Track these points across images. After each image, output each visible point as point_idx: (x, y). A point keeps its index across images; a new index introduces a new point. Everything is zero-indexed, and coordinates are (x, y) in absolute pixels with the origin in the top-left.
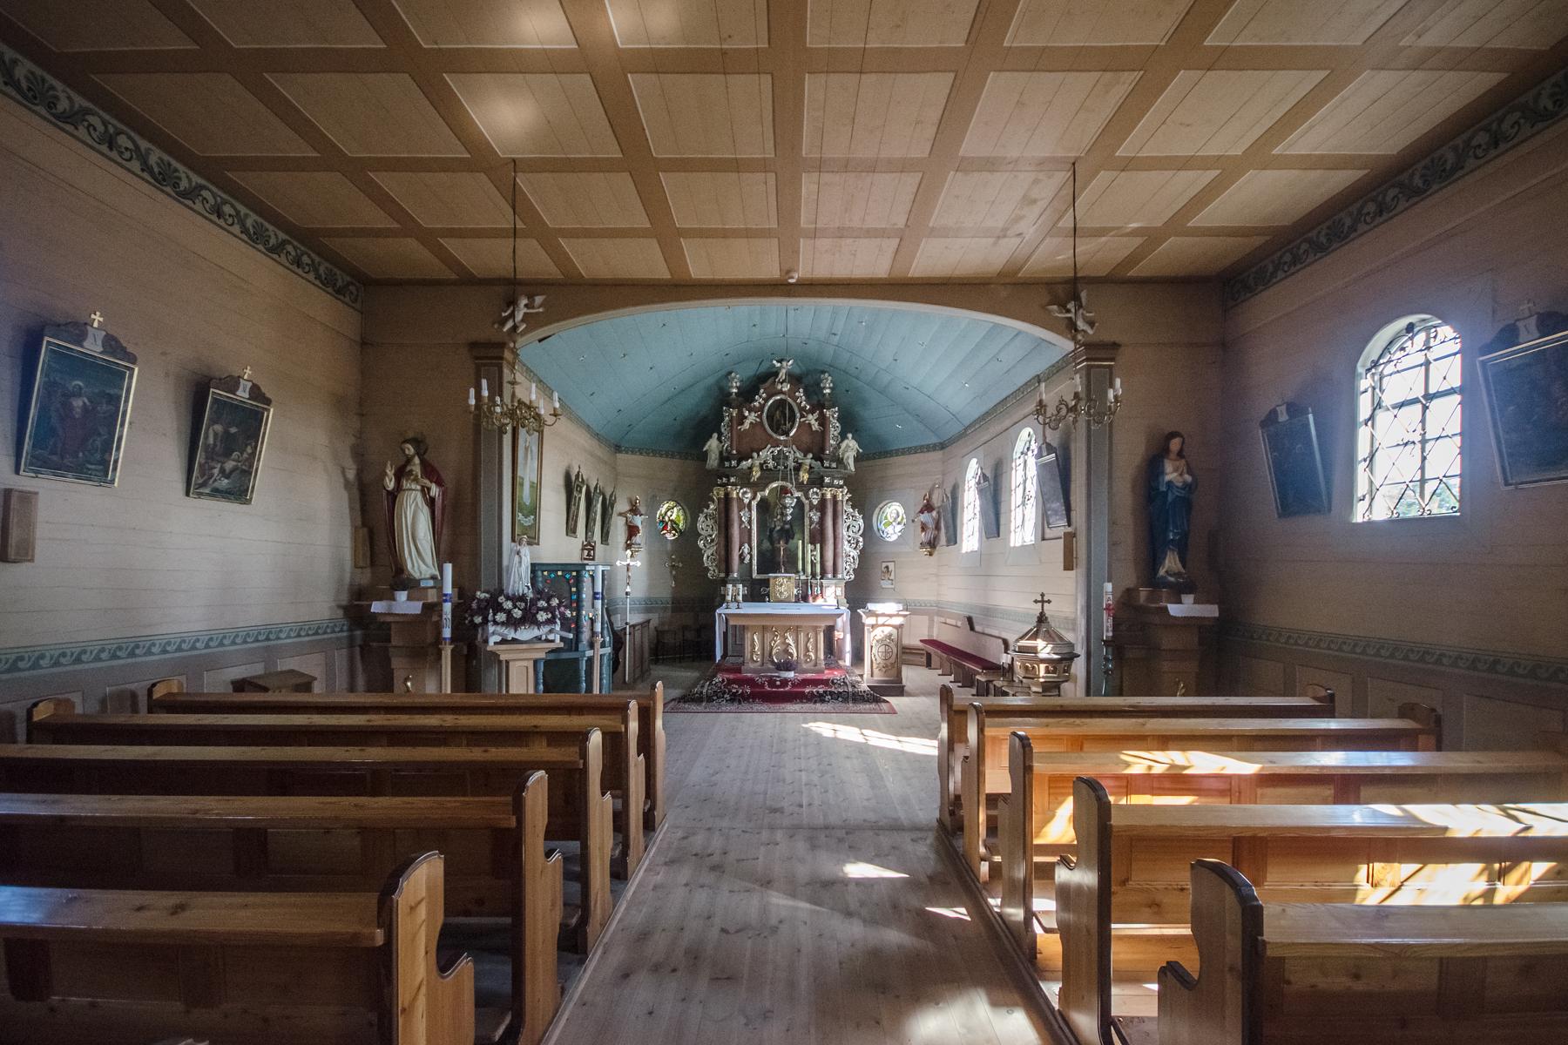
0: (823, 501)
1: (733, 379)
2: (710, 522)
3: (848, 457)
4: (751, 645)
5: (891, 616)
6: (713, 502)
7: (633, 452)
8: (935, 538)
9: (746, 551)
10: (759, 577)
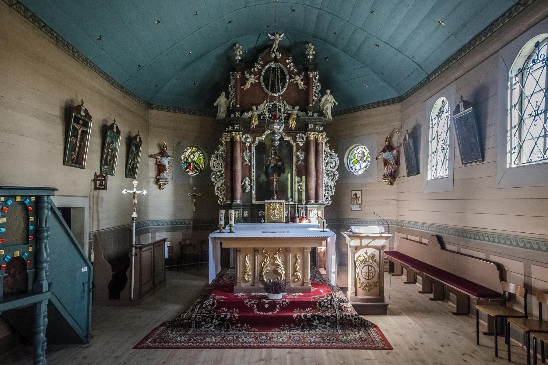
0: (307, 144)
1: (237, 49)
2: (220, 161)
3: (327, 109)
4: (243, 266)
5: (374, 238)
6: (222, 144)
7: (163, 109)
8: (395, 171)
9: (247, 183)
10: (258, 203)
